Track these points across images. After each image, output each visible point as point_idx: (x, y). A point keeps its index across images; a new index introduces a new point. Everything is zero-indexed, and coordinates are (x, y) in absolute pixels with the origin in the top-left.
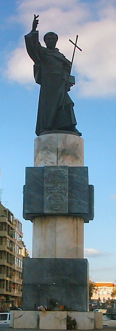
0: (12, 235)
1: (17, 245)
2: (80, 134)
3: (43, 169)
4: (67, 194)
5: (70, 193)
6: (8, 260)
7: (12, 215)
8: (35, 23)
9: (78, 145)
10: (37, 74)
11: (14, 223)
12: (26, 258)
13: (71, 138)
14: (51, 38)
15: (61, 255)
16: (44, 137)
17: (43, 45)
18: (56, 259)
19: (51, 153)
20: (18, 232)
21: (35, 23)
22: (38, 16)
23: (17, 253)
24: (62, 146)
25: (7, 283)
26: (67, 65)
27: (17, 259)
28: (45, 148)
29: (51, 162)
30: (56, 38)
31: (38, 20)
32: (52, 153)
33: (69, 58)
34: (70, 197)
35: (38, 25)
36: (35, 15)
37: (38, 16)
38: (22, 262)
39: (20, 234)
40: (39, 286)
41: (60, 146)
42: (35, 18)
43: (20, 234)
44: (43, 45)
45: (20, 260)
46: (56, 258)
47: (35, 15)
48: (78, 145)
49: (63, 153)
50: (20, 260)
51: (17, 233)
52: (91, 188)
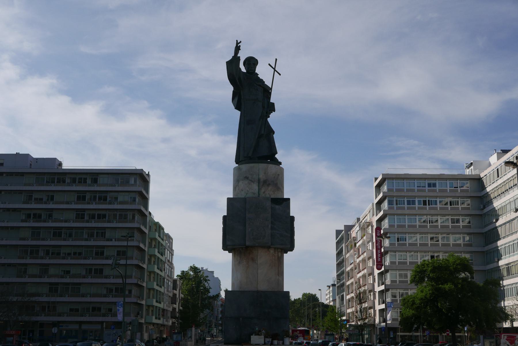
0: (162, 253)
1: (167, 265)
2: (280, 163)
3: (245, 200)
4: (270, 226)
5: (272, 225)
6: (157, 282)
7: (162, 229)
8: (238, 49)
9: (279, 175)
10: (236, 99)
11: (165, 238)
12: (226, 291)
13: (272, 167)
14: (252, 62)
15: (263, 287)
16: (245, 167)
17: (243, 69)
18: (258, 292)
19: (252, 183)
20: (168, 249)
21: (238, 49)
22: (241, 42)
23: (167, 273)
24: (263, 176)
25: (159, 310)
26: (267, 91)
27: (167, 281)
28: (246, 178)
29: (253, 193)
30: (256, 62)
31: (240, 46)
32: (254, 183)
33: (268, 83)
34: (272, 228)
35: (239, 51)
36: (237, 41)
37: (241, 42)
38: (172, 284)
39: (170, 251)
40: (241, 319)
41: (262, 176)
42: (237, 43)
43: (170, 251)
44: (243, 69)
45: (170, 283)
46: (257, 291)
47: (237, 41)
48: (279, 175)
49: (264, 183)
50: (170, 283)
51: (167, 250)
52: (293, 218)
